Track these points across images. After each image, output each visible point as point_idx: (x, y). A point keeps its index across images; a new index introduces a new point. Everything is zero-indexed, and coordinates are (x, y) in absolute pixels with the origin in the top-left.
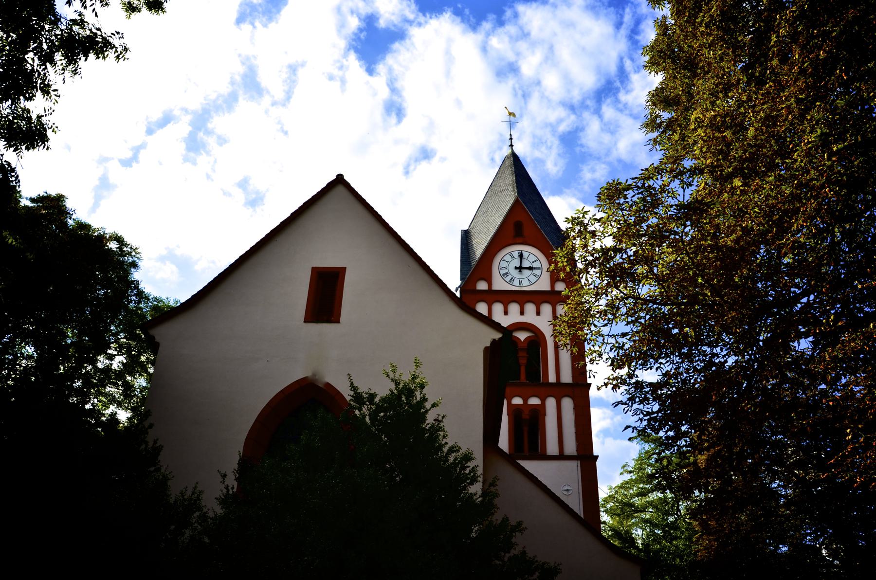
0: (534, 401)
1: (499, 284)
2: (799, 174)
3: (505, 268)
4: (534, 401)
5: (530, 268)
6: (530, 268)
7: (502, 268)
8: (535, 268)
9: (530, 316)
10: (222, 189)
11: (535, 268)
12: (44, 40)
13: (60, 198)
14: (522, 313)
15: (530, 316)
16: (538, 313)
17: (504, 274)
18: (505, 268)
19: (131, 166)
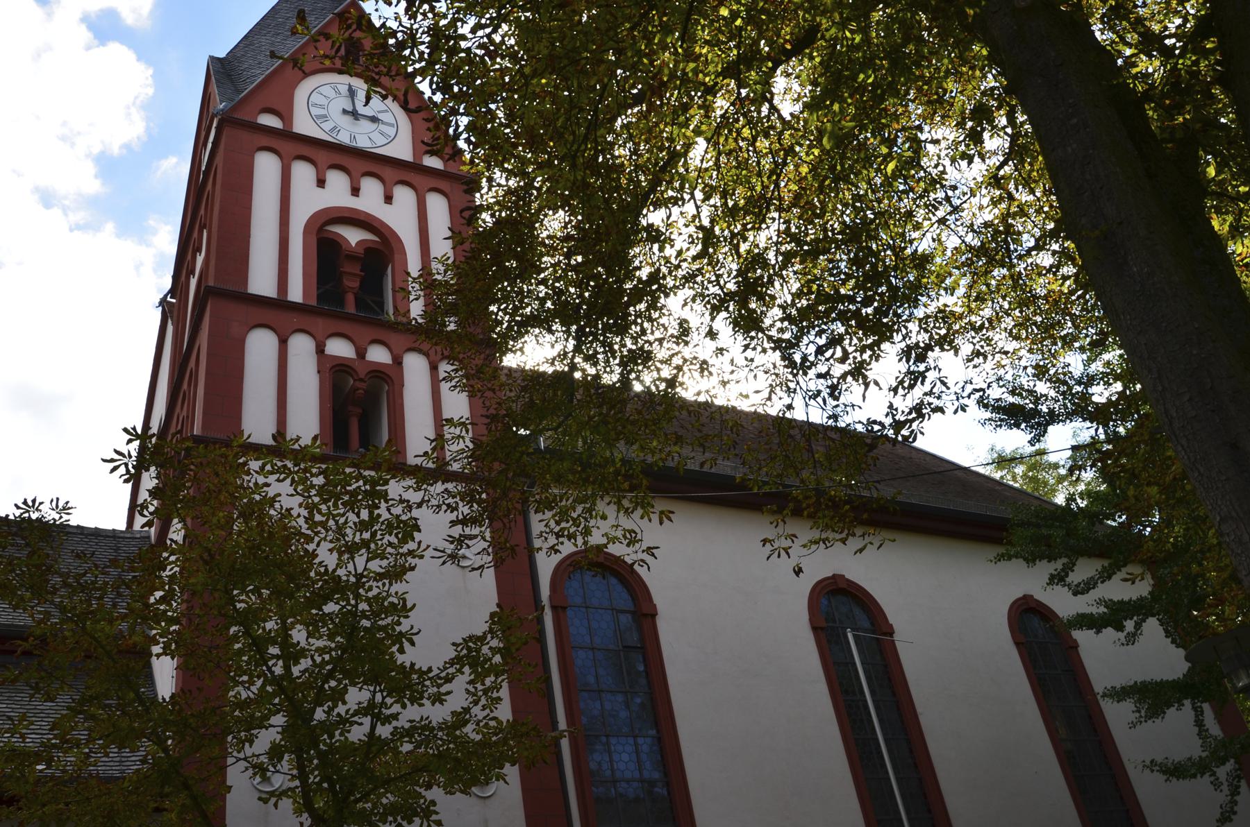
0: (378, 355)
1: (303, 125)
2: (1224, 104)
3: (321, 107)
4: (378, 355)
5: (374, 119)
6: (374, 119)
7: (315, 105)
8: (383, 123)
9: (370, 199)
10: (856, 553)
11: (383, 123)
12: (588, 506)
13: (213, 60)
14: (355, 191)
15: (370, 199)
16: (388, 199)
17: (319, 117)
18: (321, 107)
19: (1166, 637)
